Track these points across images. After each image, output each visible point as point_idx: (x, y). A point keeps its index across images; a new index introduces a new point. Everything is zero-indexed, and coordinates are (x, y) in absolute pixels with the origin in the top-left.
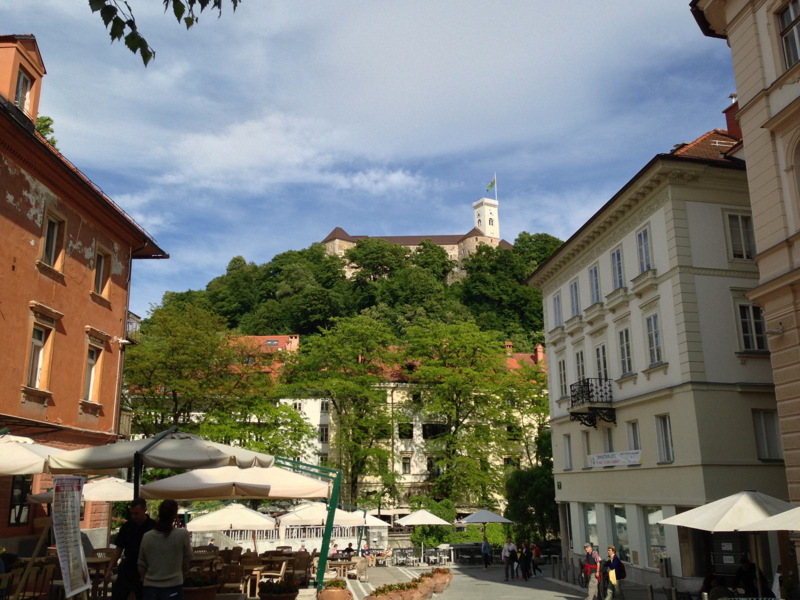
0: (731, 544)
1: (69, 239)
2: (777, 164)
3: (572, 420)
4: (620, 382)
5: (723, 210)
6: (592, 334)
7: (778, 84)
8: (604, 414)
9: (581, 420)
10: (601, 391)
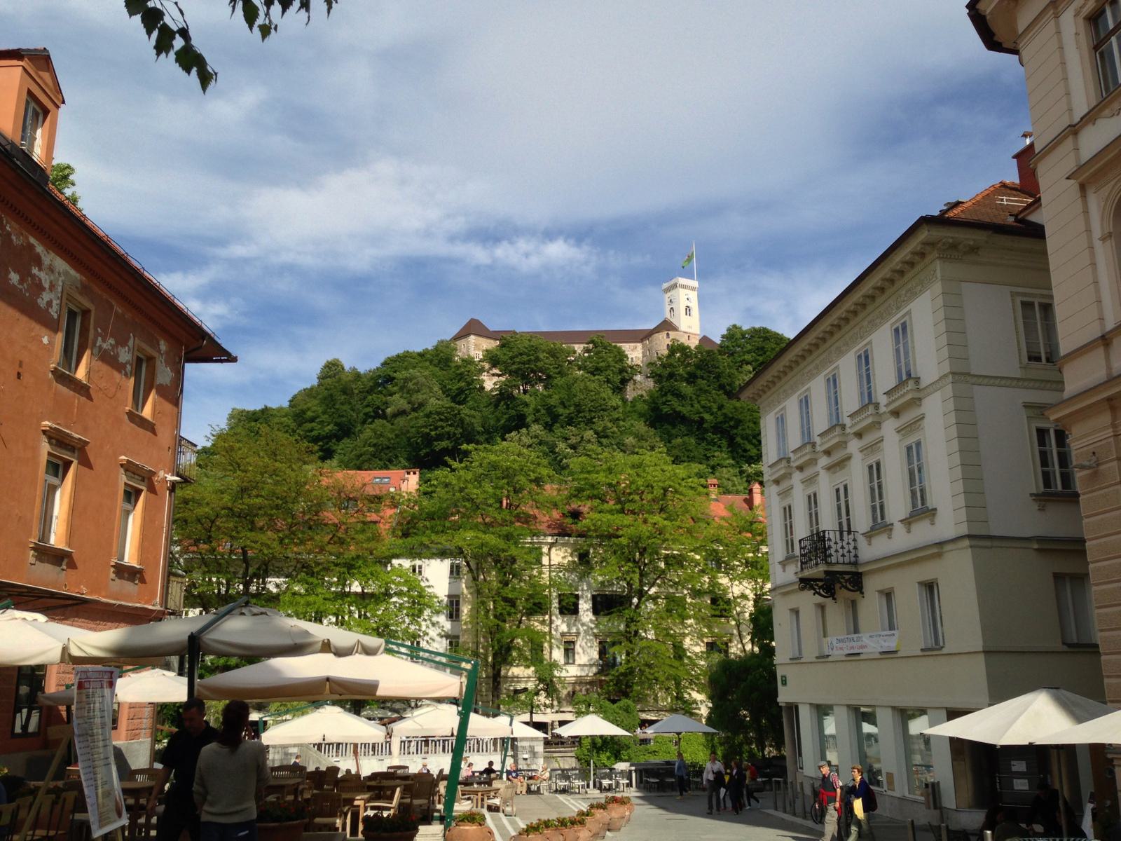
0: (1024, 763)
1: (97, 335)
2: (1088, 230)
3: (802, 589)
4: (869, 536)
5: (1013, 294)
6: (829, 468)
7: (1090, 117)
8: (846, 581)
9: (814, 589)
10: (842, 547)
